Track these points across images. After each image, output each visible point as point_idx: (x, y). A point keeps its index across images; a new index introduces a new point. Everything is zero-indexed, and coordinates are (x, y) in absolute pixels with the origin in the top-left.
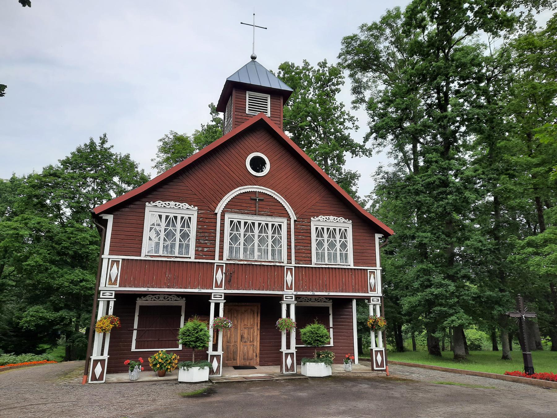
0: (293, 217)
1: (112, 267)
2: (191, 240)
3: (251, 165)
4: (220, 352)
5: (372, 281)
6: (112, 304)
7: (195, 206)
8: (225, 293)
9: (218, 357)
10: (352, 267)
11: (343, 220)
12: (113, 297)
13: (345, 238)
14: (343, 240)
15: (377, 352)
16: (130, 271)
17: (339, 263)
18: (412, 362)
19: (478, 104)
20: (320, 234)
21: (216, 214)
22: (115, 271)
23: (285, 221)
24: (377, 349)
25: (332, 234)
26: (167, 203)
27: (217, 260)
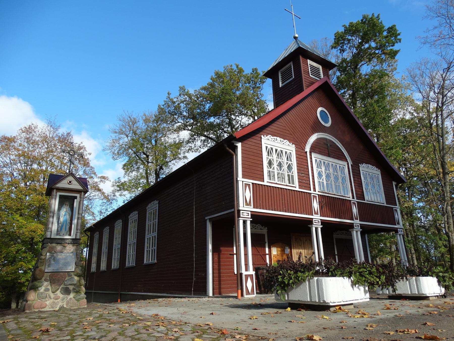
0: (350, 163)
1: (245, 189)
2: (294, 172)
3: (329, 121)
4: (252, 272)
5: (396, 216)
6: (248, 223)
7: (293, 144)
8: (321, 220)
9: (251, 276)
10: (297, 189)
11: (376, 169)
12: (250, 217)
13: (291, 160)
14: (289, 162)
15: (247, 276)
16: (262, 194)
17: (284, 184)
18: (181, 296)
19: (435, 110)
20: (269, 153)
21: (306, 152)
22: (249, 194)
23: (345, 163)
24: (247, 273)
25: (280, 154)
26: (275, 138)
27: (312, 191)
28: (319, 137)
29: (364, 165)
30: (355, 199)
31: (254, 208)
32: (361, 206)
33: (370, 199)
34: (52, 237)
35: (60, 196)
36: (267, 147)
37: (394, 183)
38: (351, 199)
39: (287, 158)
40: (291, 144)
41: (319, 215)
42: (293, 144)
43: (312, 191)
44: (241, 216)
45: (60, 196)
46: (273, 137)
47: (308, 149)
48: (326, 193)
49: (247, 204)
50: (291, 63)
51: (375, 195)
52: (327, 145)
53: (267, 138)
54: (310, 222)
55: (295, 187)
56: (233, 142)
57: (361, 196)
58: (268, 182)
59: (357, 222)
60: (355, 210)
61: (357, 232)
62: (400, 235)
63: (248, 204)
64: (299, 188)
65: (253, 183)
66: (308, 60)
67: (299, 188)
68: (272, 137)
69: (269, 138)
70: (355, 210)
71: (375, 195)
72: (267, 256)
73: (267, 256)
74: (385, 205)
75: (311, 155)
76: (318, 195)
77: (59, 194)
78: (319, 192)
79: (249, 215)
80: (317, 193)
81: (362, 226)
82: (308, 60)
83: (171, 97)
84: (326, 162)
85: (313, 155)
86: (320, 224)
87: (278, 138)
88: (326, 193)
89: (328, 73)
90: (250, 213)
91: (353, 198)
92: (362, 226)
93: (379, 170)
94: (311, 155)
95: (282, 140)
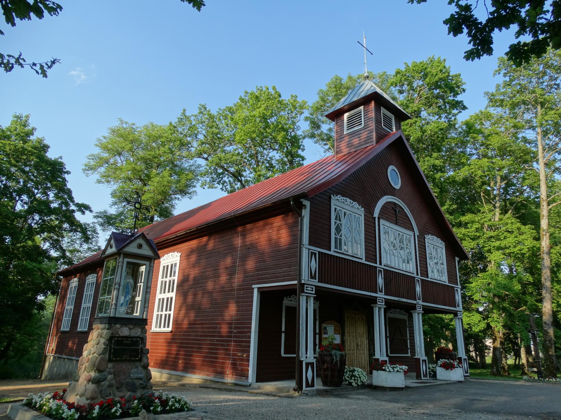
0: (417, 233)
5: (457, 297)
7: (362, 207)
23: (411, 233)
26: (345, 198)
28: (389, 200)
29: (339, 197)
30: (419, 277)
31: (319, 282)
32: (424, 283)
33: (404, 268)
34: (117, 316)
35: (128, 263)
36: (335, 209)
37: (457, 259)
38: (415, 275)
39: (336, 217)
40: (360, 207)
41: (383, 293)
42: (362, 207)
43: (378, 265)
44: (305, 291)
45: (128, 263)
46: (343, 198)
47: (376, 214)
48: (391, 267)
49: (312, 277)
50: (362, 108)
51: (438, 272)
52: (396, 211)
53: (336, 198)
54: (374, 300)
55: (361, 259)
56: (302, 200)
57: (425, 272)
58: (334, 251)
59: (381, 295)
60: (418, 289)
61: (380, 309)
62: (418, 314)
63: (313, 277)
64: (366, 260)
65: (319, 252)
66: (382, 108)
67: (366, 260)
68: (342, 198)
69: (339, 198)
70: (418, 289)
71: (438, 272)
72: (388, 335)
73: (388, 335)
74: (447, 284)
75: (379, 222)
76: (384, 269)
77: (126, 260)
78: (384, 265)
79: (312, 291)
80: (383, 267)
81: (387, 302)
82: (382, 108)
83: (187, 114)
84: (348, 212)
85: (382, 221)
86: (384, 304)
87: (348, 200)
88: (391, 267)
89: (400, 125)
90: (314, 287)
91: (418, 275)
92: (387, 302)
93: (444, 243)
94: (379, 222)
95: (352, 201)
